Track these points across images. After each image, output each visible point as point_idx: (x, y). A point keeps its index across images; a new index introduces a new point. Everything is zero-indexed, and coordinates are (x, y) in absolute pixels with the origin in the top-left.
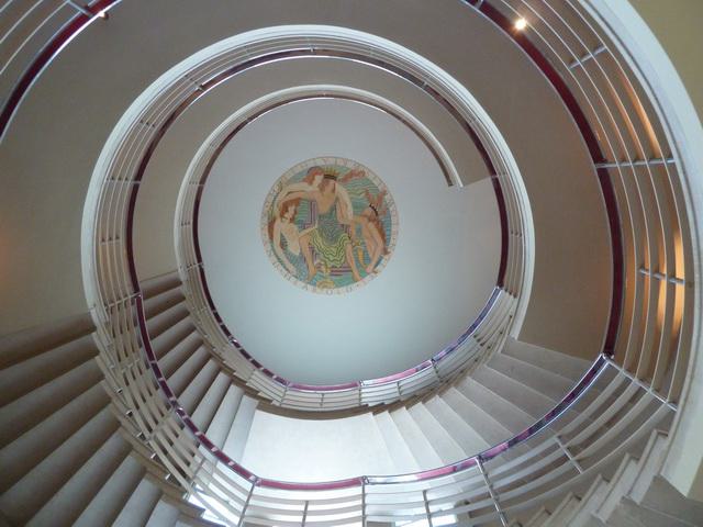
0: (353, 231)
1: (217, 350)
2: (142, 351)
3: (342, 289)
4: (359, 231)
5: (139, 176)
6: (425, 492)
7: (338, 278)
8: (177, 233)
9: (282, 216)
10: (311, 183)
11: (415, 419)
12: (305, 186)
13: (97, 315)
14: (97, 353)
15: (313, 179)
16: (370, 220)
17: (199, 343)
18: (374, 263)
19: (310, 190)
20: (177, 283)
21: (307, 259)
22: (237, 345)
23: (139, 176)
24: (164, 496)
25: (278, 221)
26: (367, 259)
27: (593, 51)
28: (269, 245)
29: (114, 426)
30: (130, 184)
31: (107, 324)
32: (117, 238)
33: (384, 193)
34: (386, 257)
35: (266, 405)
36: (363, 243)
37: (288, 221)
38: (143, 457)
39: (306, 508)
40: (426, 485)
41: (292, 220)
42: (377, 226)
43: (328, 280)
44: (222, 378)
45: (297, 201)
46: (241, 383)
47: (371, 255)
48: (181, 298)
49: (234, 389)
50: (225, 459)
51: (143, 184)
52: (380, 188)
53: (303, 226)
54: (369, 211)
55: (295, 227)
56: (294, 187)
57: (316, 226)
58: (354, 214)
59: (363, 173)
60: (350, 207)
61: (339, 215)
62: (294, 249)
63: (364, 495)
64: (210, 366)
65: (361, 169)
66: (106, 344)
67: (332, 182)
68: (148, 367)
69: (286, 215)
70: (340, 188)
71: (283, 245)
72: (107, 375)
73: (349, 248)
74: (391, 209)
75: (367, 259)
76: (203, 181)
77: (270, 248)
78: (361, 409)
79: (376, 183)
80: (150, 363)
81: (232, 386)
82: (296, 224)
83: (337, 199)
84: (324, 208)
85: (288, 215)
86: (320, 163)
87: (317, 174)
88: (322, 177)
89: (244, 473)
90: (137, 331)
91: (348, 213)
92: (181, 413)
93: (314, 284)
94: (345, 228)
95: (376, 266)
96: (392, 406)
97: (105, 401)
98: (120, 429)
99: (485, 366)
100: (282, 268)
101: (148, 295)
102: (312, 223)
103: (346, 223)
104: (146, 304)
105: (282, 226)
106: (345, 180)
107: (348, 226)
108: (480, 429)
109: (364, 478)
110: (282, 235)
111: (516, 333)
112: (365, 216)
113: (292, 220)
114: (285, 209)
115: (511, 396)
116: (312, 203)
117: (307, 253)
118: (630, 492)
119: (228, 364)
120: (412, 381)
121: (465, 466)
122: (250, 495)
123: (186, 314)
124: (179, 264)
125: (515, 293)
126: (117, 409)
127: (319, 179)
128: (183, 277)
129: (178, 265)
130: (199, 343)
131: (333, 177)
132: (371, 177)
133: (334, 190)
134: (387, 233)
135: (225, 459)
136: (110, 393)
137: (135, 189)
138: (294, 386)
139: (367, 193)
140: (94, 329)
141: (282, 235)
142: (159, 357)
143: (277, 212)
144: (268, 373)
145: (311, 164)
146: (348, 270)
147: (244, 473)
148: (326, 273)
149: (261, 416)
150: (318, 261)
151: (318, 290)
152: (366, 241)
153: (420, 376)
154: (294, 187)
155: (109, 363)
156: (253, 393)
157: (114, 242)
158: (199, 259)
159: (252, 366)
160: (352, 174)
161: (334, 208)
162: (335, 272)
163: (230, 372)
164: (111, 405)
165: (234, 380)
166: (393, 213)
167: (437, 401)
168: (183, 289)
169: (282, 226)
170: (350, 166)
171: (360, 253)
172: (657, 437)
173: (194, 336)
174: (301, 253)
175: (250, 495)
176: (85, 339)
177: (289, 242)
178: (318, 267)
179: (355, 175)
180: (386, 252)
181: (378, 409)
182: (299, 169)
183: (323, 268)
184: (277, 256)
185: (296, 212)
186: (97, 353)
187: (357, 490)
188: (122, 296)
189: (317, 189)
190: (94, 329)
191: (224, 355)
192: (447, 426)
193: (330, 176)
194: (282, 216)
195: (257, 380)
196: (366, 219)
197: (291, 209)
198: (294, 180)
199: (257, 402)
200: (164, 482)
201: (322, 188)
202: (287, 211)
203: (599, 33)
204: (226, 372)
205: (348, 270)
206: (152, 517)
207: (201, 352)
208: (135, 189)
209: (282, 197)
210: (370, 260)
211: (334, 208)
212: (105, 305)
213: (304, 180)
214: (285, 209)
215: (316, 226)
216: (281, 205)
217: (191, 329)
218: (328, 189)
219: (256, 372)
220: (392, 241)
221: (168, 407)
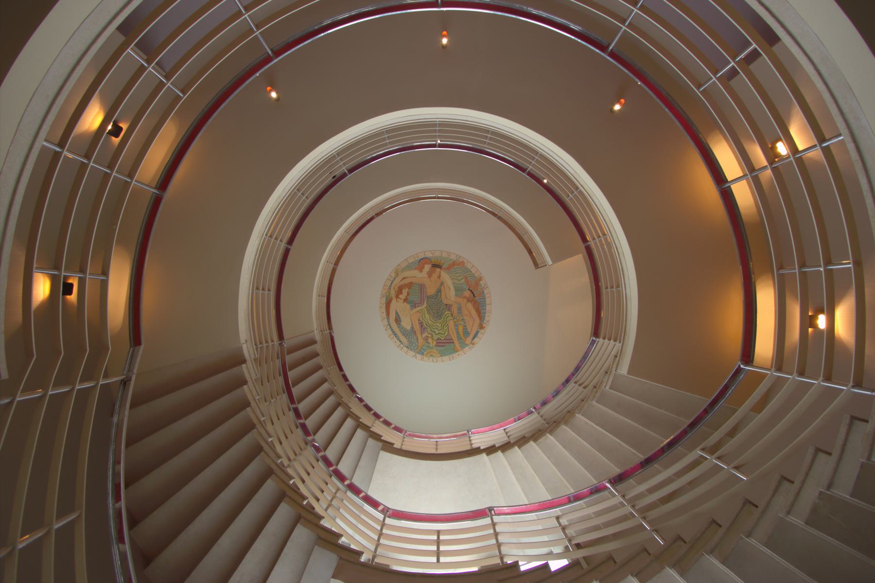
0: (455, 309)
1: (345, 399)
2: (285, 396)
3: (446, 358)
4: (460, 309)
5: (291, 241)
6: (558, 518)
7: (442, 348)
8: (316, 301)
9: (397, 297)
10: (421, 271)
11: (526, 458)
12: (416, 273)
13: (248, 351)
14: (245, 382)
15: (423, 268)
16: (468, 301)
17: (330, 393)
18: (471, 336)
19: (421, 276)
20: (313, 342)
21: (417, 332)
22: (361, 400)
23: (291, 241)
24: (302, 520)
25: (394, 301)
26: (466, 333)
27: (734, 59)
28: (386, 320)
29: (257, 450)
30: (283, 245)
31: (255, 360)
32: (269, 290)
33: (480, 279)
34: (482, 331)
35: (388, 447)
36: (463, 320)
37: (402, 300)
38: (283, 482)
39: (438, 537)
40: (557, 511)
41: (405, 300)
42: (474, 305)
43: (434, 350)
44: (349, 423)
45: (410, 285)
46: (366, 428)
47: (469, 330)
48: (316, 355)
49: (360, 434)
50: (356, 490)
51: (293, 248)
52: (476, 275)
53: (414, 305)
54: (467, 294)
55: (408, 306)
56: (407, 274)
57: (425, 305)
58: (456, 295)
59: (463, 263)
60: (452, 288)
61: (443, 297)
62: (406, 324)
63: (494, 525)
64: (339, 413)
65: (461, 260)
66: (254, 377)
67: (438, 270)
68: (290, 410)
69: (400, 296)
70: (445, 276)
71: (398, 320)
72: (253, 404)
73: (451, 323)
74: (485, 292)
75: (466, 333)
76: (337, 263)
77: (387, 323)
78: (474, 452)
79: (473, 271)
80: (292, 406)
81: (299, 526)
82: (408, 303)
83: (442, 284)
84: (431, 291)
85: (402, 296)
86: (429, 255)
87: (426, 263)
88: (430, 266)
89: (375, 504)
90: (281, 379)
91: (450, 295)
92: (317, 449)
93: (423, 354)
94: (448, 307)
95: (474, 338)
96: (505, 447)
97: (249, 427)
98: (262, 453)
99: (594, 403)
100: (395, 339)
101: (291, 351)
102: (421, 303)
103: (449, 303)
104: (289, 359)
105: (397, 305)
106: (448, 268)
107: (451, 306)
108: (589, 466)
109: (490, 509)
110: (397, 313)
111: (624, 369)
112: (465, 297)
113: (405, 300)
114: (400, 291)
115: (617, 431)
116: (422, 287)
117: (417, 328)
118: (829, 486)
119: (353, 411)
120: (516, 428)
121: (597, 489)
122: (383, 525)
123: (319, 368)
124: (315, 326)
125: (618, 336)
126: (261, 435)
127: (427, 267)
128: (318, 337)
129: (314, 326)
130: (330, 393)
131: (439, 266)
132: (469, 266)
133: (439, 277)
134: (482, 311)
135: (356, 490)
136: (255, 421)
137: (287, 252)
138: (410, 435)
139: (466, 278)
140: (244, 361)
141: (397, 313)
142: (299, 402)
143: (393, 293)
144: (387, 423)
145: (421, 256)
146: (450, 341)
147: (375, 504)
148: (431, 342)
149: (385, 456)
150: (426, 334)
151: (426, 358)
152: (465, 318)
153: (516, 426)
154: (407, 274)
155: (255, 393)
156: (377, 437)
157: (278, 242)
158: (330, 328)
159: (373, 418)
160: (454, 264)
161: (439, 291)
162: (440, 343)
163: (356, 418)
164: (255, 430)
165: (359, 425)
166: (487, 296)
167: (550, 438)
168: (317, 347)
169: (396, 305)
170: (453, 257)
171: (461, 328)
172: (850, 426)
173: (326, 386)
174: (412, 328)
175: (383, 525)
176: (235, 370)
177: (402, 318)
178: (426, 339)
179: (456, 265)
180: (481, 327)
181: (491, 450)
182: (411, 260)
183: (430, 340)
184: (392, 330)
185: (408, 294)
186: (245, 382)
187: (487, 521)
188: (270, 341)
189: (427, 276)
190: (244, 361)
191: (350, 405)
192: (558, 463)
193: (436, 266)
194: (397, 297)
195: (378, 428)
196: (465, 301)
197: (405, 291)
198: (409, 267)
199: (380, 444)
200: (303, 507)
201: (430, 274)
202: (401, 293)
203: (592, 226)
204: (352, 418)
205: (450, 341)
206: (289, 543)
207: (331, 401)
208: (287, 252)
209: (398, 282)
210: (469, 334)
211: (439, 291)
212: (256, 345)
213: (416, 269)
214: (400, 291)
215: (425, 305)
216: (396, 288)
217: (324, 381)
218: (435, 276)
219: (377, 422)
220: (487, 318)
221: (306, 444)
